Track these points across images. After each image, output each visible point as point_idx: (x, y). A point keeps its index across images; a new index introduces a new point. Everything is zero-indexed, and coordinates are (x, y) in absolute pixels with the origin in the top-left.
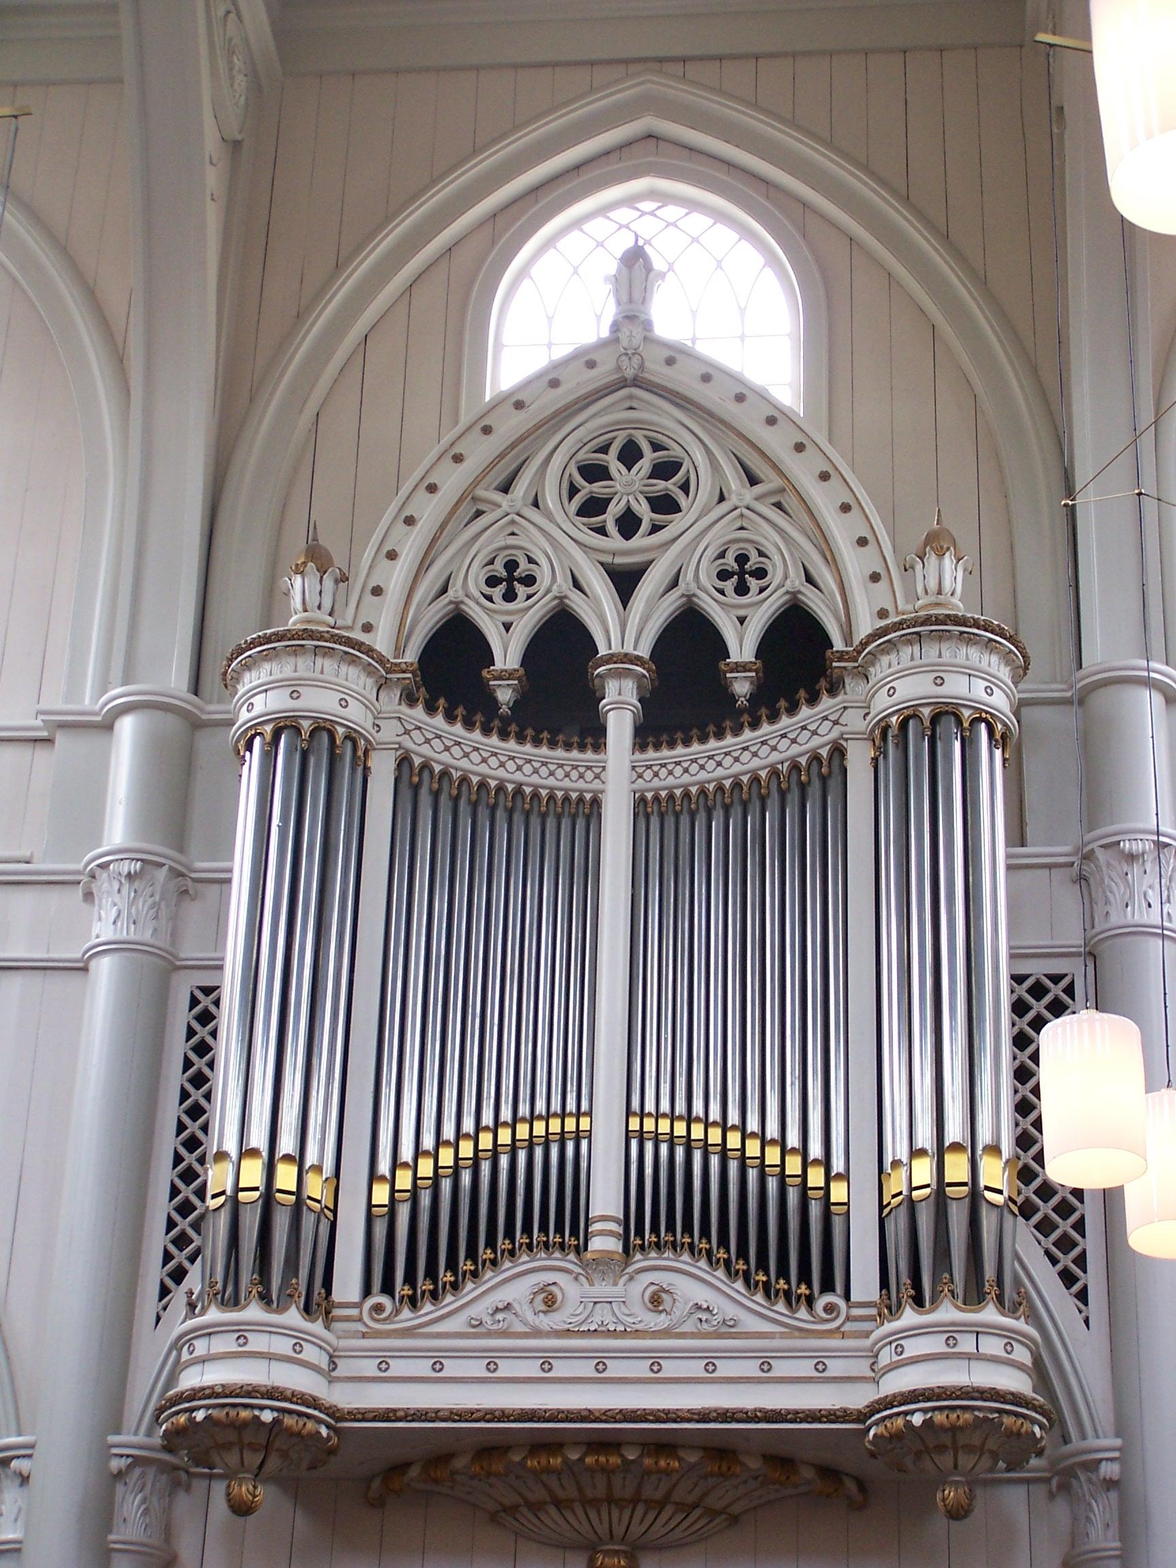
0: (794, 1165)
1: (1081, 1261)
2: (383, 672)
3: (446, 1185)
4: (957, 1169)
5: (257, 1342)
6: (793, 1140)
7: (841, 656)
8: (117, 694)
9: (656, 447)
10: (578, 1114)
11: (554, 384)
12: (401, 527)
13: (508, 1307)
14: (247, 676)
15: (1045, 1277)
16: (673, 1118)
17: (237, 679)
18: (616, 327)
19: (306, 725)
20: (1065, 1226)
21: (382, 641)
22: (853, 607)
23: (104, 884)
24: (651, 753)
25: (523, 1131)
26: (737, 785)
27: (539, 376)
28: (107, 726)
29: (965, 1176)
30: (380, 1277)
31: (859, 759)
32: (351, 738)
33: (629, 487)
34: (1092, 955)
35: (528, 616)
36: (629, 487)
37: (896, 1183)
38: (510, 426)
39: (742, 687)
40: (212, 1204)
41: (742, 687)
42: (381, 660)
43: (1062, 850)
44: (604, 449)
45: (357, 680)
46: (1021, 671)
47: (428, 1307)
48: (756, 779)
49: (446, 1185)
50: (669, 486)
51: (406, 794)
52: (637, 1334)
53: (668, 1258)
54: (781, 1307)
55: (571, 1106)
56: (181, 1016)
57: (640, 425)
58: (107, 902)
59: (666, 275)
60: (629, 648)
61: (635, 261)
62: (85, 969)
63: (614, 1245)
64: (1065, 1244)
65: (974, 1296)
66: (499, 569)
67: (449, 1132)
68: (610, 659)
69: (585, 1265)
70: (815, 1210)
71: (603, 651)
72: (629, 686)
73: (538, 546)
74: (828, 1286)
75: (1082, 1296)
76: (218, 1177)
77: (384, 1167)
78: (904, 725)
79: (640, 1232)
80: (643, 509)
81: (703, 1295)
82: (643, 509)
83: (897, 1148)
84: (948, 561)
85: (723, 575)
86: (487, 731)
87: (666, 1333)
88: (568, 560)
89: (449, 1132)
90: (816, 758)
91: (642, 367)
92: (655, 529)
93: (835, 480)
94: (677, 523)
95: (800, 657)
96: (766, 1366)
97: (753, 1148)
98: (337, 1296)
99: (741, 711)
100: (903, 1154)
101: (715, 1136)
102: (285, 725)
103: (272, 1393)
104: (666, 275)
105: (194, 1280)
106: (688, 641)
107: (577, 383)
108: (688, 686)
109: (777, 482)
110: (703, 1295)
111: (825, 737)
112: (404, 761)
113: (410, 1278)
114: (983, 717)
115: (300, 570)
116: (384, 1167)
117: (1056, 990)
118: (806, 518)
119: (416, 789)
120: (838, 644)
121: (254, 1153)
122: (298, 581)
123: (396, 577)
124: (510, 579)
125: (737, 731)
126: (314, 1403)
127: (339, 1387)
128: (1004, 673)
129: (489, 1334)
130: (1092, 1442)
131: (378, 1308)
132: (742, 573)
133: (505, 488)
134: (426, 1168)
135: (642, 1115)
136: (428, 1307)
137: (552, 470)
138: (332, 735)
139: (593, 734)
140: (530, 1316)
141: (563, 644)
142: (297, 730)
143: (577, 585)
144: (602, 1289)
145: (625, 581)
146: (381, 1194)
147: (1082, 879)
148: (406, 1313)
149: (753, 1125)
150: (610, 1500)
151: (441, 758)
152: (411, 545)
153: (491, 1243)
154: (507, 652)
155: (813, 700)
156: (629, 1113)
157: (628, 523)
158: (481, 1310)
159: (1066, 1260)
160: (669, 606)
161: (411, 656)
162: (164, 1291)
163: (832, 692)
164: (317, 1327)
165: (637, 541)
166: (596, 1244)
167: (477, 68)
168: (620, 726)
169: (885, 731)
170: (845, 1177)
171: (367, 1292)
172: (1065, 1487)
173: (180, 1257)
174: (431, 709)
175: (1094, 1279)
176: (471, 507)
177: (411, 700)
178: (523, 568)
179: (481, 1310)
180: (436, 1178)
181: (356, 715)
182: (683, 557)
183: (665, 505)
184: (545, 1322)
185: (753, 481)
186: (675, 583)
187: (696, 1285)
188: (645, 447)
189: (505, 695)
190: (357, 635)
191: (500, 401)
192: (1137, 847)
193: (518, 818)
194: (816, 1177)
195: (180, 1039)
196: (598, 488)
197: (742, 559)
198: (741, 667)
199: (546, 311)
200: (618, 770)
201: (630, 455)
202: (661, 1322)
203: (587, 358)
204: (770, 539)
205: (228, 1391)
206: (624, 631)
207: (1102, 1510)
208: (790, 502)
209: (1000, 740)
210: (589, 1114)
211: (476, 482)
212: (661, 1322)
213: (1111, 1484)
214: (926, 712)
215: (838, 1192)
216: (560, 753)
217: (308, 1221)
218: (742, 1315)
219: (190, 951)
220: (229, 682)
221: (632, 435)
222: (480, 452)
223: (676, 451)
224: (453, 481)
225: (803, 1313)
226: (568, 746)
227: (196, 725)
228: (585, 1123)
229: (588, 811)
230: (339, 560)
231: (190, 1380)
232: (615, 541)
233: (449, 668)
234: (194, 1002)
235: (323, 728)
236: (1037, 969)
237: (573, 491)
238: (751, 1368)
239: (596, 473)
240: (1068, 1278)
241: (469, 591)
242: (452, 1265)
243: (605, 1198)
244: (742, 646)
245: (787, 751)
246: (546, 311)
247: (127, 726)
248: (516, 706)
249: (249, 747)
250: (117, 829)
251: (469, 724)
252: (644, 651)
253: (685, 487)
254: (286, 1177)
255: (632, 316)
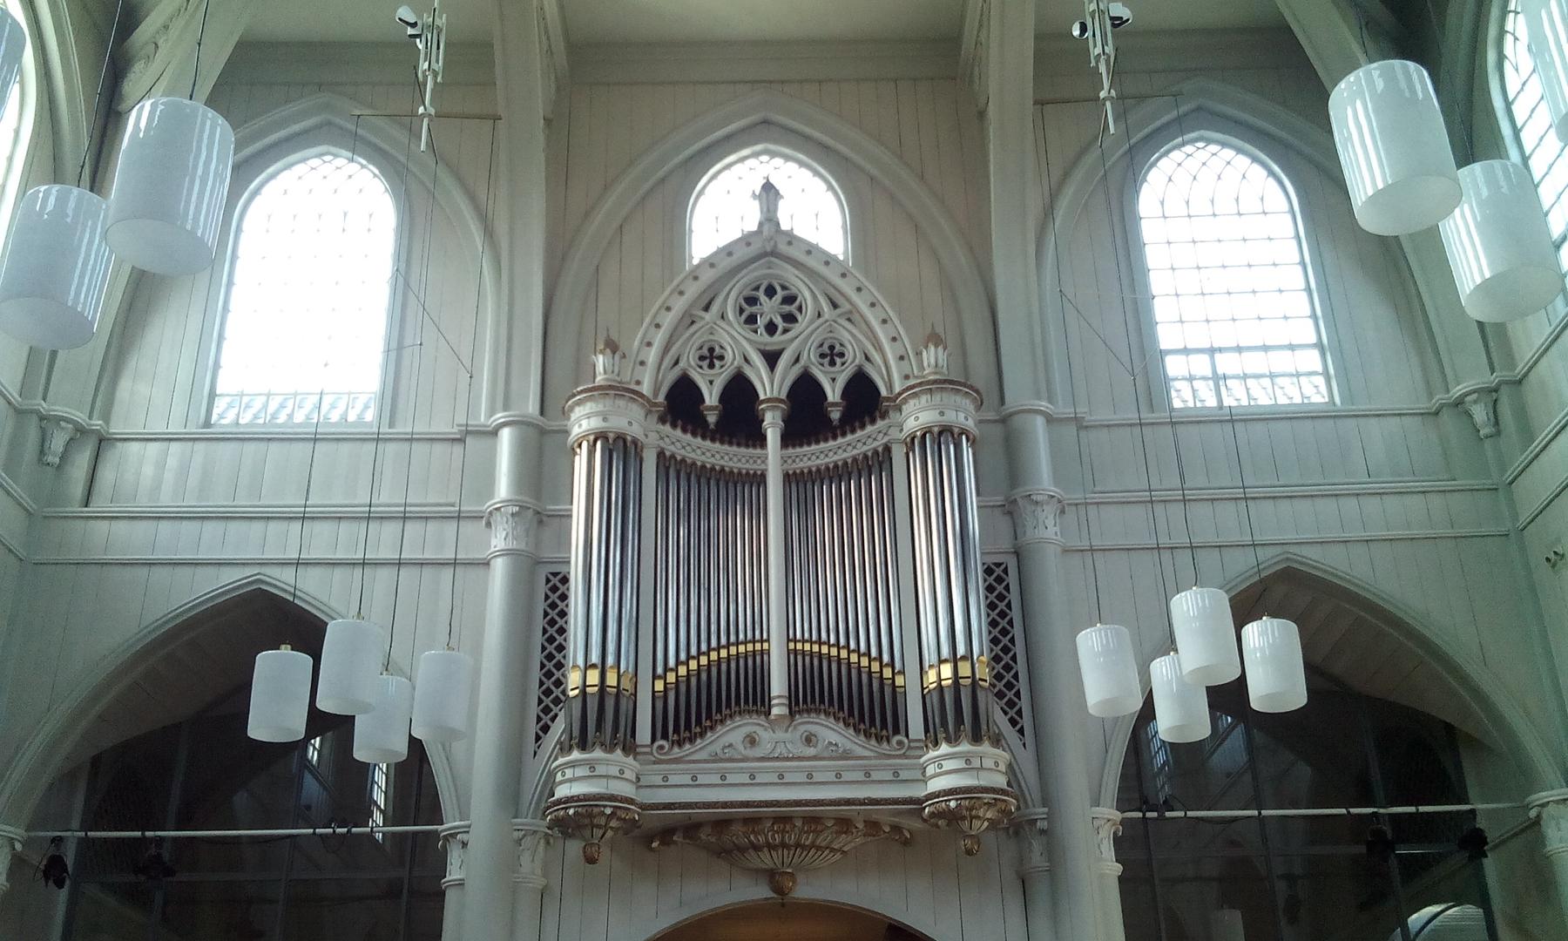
0: (875, 667)
1: (1019, 713)
2: (648, 404)
3: (694, 681)
4: (965, 669)
5: (600, 770)
6: (874, 653)
7: (888, 399)
8: (500, 417)
9: (784, 288)
10: (762, 641)
11: (730, 254)
12: (653, 328)
13: (730, 745)
14: (577, 409)
15: (1001, 721)
16: (812, 643)
17: (572, 409)
18: (761, 224)
19: (611, 436)
20: (1010, 695)
21: (646, 389)
22: (889, 376)
23: (497, 516)
24: (667, 428)
25: (733, 650)
26: (836, 466)
27: (809, 244)
28: (495, 433)
29: (969, 674)
30: (660, 730)
31: (898, 454)
32: (635, 442)
33: (769, 309)
34: (1017, 554)
35: (721, 377)
36: (769, 309)
37: (932, 676)
38: (708, 276)
39: (835, 415)
40: (572, 694)
41: (835, 415)
42: (648, 401)
43: (999, 500)
44: (757, 289)
45: (636, 411)
46: (980, 405)
47: (687, 746)
48: (846, 463)
49: (694, 681)
50: (792, 308)
51: (662, 468)
52: (800, 759)
53: (813, 717)
54: (873, 742)
55: (758, 636)
56: (542, 589)
57: (777, 277)
58: (500, 528)
59: (762, 198)
60: (775, 394)
61: (769, 193)
62: (487, 564)
63: (785, 711)
64: (1011, 704)
65: (976, 738)
66: (705, 352)
67: (694, 651)
68: (768, 400)
69: (770, 722)
70: (888, 690)
71: (762, 397)
72: (778, 414)
73: (725, 340)
74: (896, 731)
75: (1021, 731)
76: (574, 679)
77: (660, 671)
78: (924, 436)
79: (797, 703)
80: (778, 321)
81: (833, 737)
82: (778, 321)
83: (930, 656)
84: (940, 349)
85: (822, 356)
86: (704, 438)
87: (815, 758)
88: (740, 346)
89: (694, 651)
90: (876, 452)
91: (775, 245)
92: (786, 331)
93: (878, 307)
94: (796, 329)
95: (865, 400)
96: (868, 774)
97: (854, 658)
98: (638, 741)
99: (835, 428)
100: (934, 660)
101: (834, 651)
102: (600, 435)
103: (612, 798)
104: (762, 198)
105: (558, 728)
106: (805, 392)
107: (742, 254)
108: (807, 416)
109: (847, 306)
110: (833, 737)
111: (878, 444)
112: (661, 454)
113: (676, 730)
114: (963, 432)
115: (602, 352)
116: (660, 671)
117: (998, 571)
118: (864, 326)
119: (667, 469)
120: (884, 392)
121: (594, 666)
122: (601, 358)
123: (652, 355)
124: (711, 357)
125: (835, 438)
126: (631, 801)
127: (642, 791)
128: (971, 408)
129: (722, 760)
130: (1032, 810)
131: (661, 747)
132: (832, 355)
133: (707, 308)
134: (682, 671)
135: (795, 641)
136: (687, 746)
137: (730, 301)
138: (625, 441)
139: (761, 440)
140: (741, 748)
141: (739, 391)
142: (607, 439)
143: (746, 360)
144: (780, 735)
145: (771, 358)
146: (659, 686)
147: (1010, 513)
148: (676, 749)
149: (853, 645)
150: (784, 845)
151: (680, 453)
152: (659, 339)
153: (719, 710)
154: (711, 397)
155: (873, 422)
156: (789, 640)
157: (771, 328)
158: (717, 747)
159: (1012, 713)
160: (795, 372)
161: (661, 399)
162: (538, 738)
163: (883, 417)
164: (630, 760)
165: (778, 337)
166: (775, 711)
167: (695, 83)
168: (773, 435)
169: (913, 440)
170: (902, 672)
171: (654, 740)
172: (1017, 833)
173: (546, 719)
174: (674, 426)
175: (1026, 721)
176: (689, 320)
177: (662, 420)
178: (718, 351)
179: (717, 747)
180: (688, 676)
181: (635, 431)
182: (800, 345)
183: (790, 318)
184: (750, 753)
185: (835, 306)
186: (797, 360)
187: (830, 732)
188: (778, 289)
189: (712, 419)
190: (633, 387)
191: (704, 262)
192: (1039, 498)
193: (722, 484)
194: (887, 673)
195: (545, 598)
196: (787, 308)
197: (832, 348)
198: (834, 404)
199: (721, 211)
200: (773, 457)
201: (770, 292)
202: (811, 751)
203: (747, 239)
204: (845, 337)
205: (586, 797)
206: (770, 385)
207: (1037, 846)
208: (856, 317)
209: (973, 442)
210: (768, 640)
211: (692, 306)
212: (811, 751)
213: (1043, 832)
214: (936, 430)
215: (899, 681)
216: (735, 448)
217: (623, 702)
218: (855, 747)
219: (547, 554)
220: (565, 414)
221: (767, 275)
222: (692, 290)
223: (794, 291)
224: (679, 305)
225: (885, 744)
226: (739, 445)
227: (543, 432)
228: (766, 646)
229: (760, 479)
230: (622, 347)
231: (562, 792)
232: (767, 338)
233: (681, 403)
234: (548, 581)
235: (621, 438)
236: (991, 560)
237: (742, 311)
238: (860, 776)
239: (752, 301)
240: (1013, 722)
241: (690, 363)
242: (709, 717)
243: (778, 685)
244: (833, 393)
245: (860, 449)
246: (721, 211)
247: (506, 433)
248: (717, 424)
249: (580, 446)
250: (503, 488)
251: (694, 434)
252: (783, 396)
253: (800, 309)
254: (611, 679)
255: (769, 217)
